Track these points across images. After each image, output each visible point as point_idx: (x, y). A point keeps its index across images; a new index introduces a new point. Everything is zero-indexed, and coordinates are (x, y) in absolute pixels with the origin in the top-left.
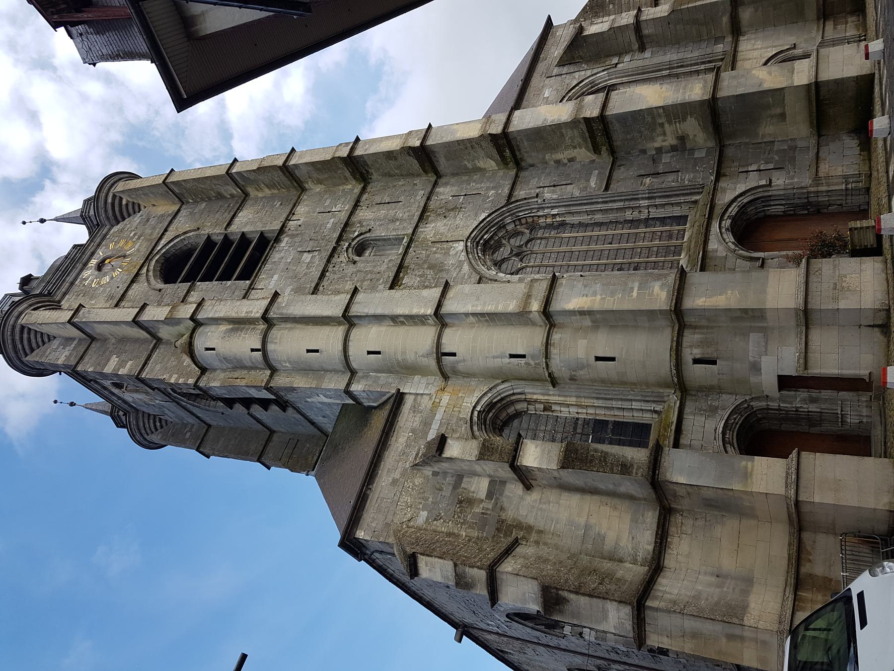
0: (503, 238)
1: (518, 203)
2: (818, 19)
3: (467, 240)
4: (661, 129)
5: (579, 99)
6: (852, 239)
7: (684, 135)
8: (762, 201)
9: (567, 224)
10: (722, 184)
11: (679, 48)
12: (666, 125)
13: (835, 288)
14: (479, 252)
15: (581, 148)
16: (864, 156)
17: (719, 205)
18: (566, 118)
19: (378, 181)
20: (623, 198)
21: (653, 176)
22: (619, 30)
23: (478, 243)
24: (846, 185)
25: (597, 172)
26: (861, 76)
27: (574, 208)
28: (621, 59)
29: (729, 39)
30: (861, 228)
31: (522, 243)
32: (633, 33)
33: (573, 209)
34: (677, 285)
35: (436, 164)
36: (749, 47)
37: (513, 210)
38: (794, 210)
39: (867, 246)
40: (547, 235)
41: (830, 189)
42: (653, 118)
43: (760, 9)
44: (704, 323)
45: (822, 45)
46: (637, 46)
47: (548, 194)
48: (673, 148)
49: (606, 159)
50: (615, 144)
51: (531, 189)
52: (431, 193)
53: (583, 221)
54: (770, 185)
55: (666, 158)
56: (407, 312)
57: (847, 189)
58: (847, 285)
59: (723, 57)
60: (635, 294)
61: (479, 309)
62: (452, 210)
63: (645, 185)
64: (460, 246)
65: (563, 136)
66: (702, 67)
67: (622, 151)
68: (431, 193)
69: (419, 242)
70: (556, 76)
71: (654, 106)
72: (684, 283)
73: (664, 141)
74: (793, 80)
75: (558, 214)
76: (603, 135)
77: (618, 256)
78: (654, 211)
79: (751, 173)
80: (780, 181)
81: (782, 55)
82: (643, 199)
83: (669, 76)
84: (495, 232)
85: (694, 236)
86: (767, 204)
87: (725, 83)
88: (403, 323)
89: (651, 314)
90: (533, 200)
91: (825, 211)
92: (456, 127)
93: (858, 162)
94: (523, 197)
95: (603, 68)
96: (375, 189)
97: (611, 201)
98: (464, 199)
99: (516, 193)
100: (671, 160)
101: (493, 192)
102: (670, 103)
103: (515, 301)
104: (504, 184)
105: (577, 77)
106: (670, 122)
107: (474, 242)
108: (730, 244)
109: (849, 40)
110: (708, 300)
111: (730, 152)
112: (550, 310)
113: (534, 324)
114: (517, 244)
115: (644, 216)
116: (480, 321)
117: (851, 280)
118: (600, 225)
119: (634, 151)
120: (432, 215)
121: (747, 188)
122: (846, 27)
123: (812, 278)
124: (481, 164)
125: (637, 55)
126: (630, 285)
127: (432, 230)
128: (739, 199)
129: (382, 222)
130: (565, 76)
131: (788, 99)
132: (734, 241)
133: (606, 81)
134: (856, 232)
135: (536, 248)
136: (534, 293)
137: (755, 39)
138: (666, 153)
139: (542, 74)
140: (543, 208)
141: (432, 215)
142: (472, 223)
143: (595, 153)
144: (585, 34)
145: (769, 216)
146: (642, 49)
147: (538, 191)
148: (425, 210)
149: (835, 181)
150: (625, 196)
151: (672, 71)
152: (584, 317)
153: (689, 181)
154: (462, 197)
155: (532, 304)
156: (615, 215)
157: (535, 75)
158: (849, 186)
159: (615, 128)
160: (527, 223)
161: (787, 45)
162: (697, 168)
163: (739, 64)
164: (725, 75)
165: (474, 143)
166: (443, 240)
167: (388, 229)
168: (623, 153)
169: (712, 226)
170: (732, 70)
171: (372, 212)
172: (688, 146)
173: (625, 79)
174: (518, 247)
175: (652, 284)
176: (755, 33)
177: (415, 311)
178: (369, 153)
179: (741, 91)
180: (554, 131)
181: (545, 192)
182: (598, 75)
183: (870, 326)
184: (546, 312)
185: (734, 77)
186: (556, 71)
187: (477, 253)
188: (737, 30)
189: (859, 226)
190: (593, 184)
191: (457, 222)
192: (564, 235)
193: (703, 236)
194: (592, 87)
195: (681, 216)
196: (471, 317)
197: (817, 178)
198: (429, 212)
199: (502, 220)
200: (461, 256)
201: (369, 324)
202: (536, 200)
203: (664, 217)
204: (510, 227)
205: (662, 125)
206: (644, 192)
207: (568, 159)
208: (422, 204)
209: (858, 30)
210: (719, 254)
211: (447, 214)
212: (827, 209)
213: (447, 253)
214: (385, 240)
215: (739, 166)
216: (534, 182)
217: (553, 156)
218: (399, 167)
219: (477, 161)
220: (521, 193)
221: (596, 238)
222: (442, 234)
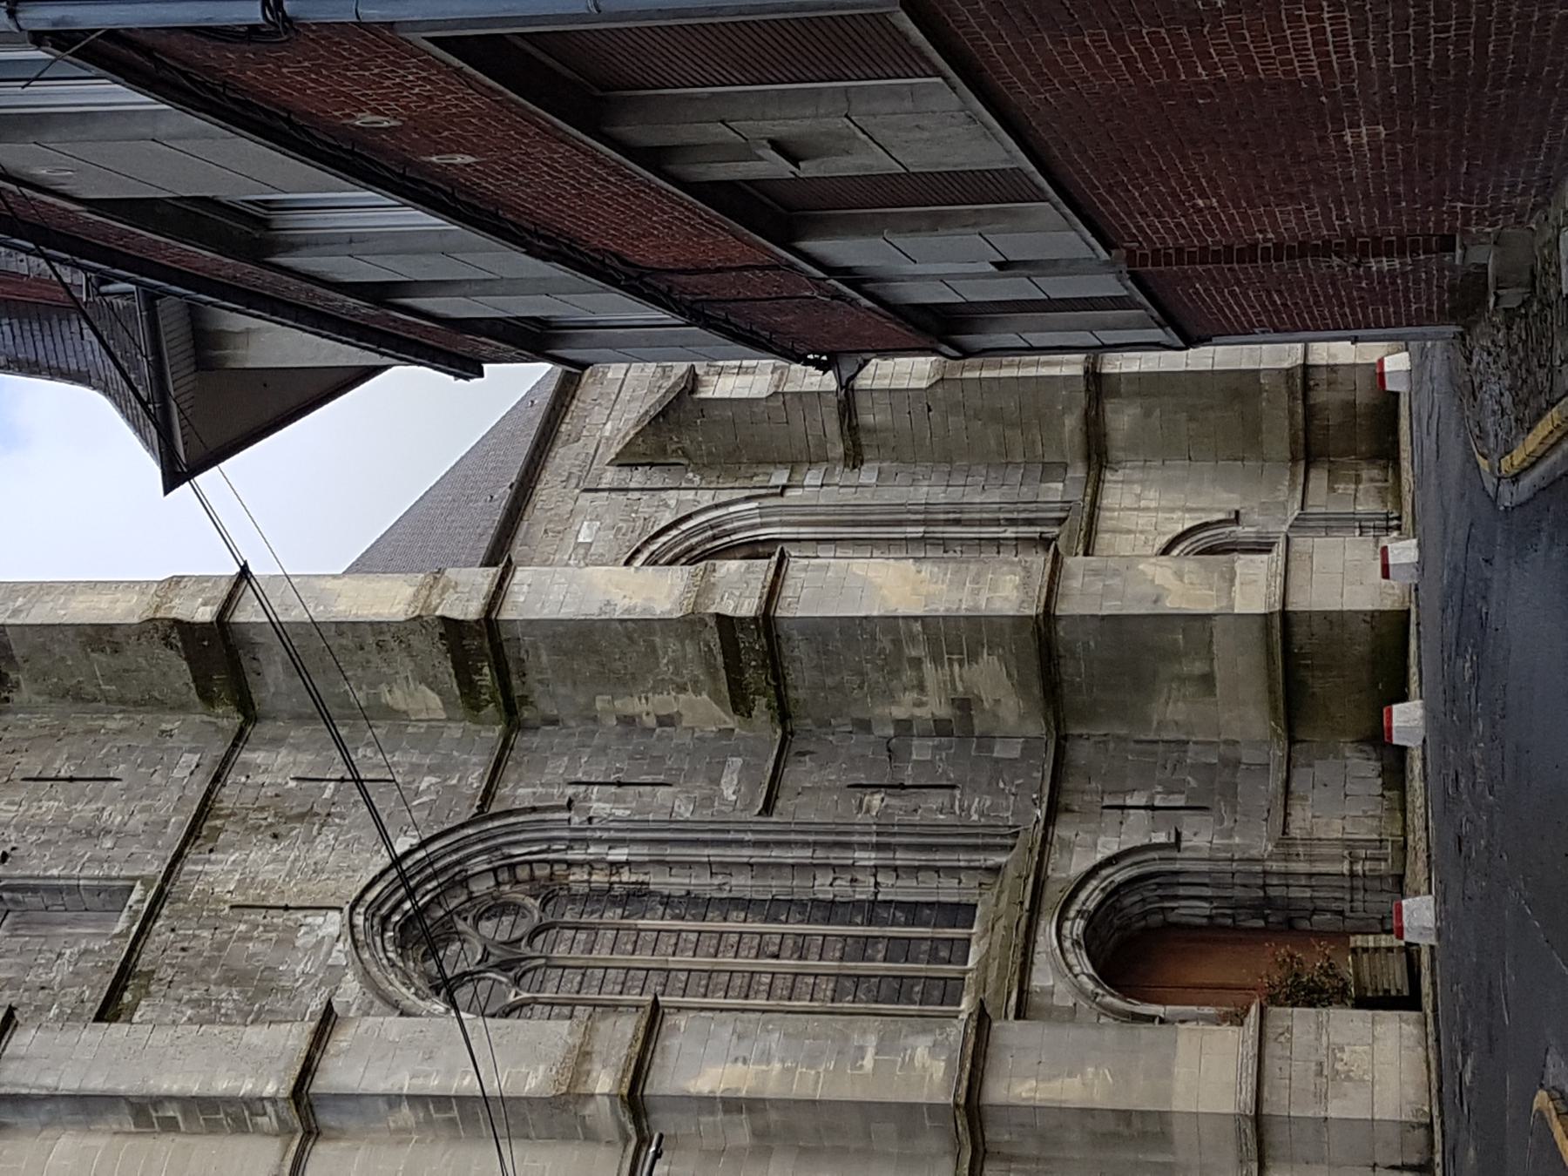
0: (459, 914)
1: (512, 820)
2: (1294, 460)
3: (353, 908)
4: (914, 674)
5: (702, 565)
6: (1357, 974)
7: (970, 696)
8: (1159, 885)
9: (651, 894)
10: (1062, 831)
11: (950, 474)
12: (928, 666)
13: (1320, 1073)
14: (390, 947)
15: (697, 692)
16: (1390, 799)
17: (1059, 880)
18: (668, 607)
19: (31, 709)
20: (811, 838)
21: (889, 791)
22: (796, 399)
23: (385, 919)
24: (1351, 863)
25: (738, 761)
26: (1382, 613)
27: (676, 851)
28: (797, 477)
29: (1078, 471)
30: (1376, 949)
31: (517, 934)
32: (835, 416)
33: (671, 852)
34: (970, 1045)
35: (251, 678)
36: (1128, 502)
37: (494, 837)
38: (1233, 917)
39: (1389, 991)
40: (594, 919)
41: (1315, 870)
42: (896, 642)
43: (1157, 412)
44: (1031, 1148)
45: (1301, 524)
46: (840, 450)
47: (601, 805)
48: (941, 728)
49: (763, 728)
50: (792, 694)
51: (551, 785)
52: (226, 763)
53: (695, 891)
54: (1177, 845)
55: (921, 750)
56: (195, 1089)
57: (1353, 875)
58: (1346, 1068)
59: (1063, 515)
60: (868, 1063)
61: (433, 1084)
62: (301, 817)
63: (868, 811)
64: (332, 924)
65: (654, 650)
66: (1010, 532)
67: (809, 716)
68: (226, 763)
69: (186, 902)
70: (611, 490)
71: (900, 612)
72: (987, 1046)
73: (920, 704)
74: (1231, 600)
75: (628, 863)
76: (764, 666)
77: (797, 991)
78: (890, 882)
79: (1132, 811)
80: (1200, 837)
81: (1206, 534)
82: (864, 846)
83: (923, 540)
84: (437, 896)
85: (996, 951)
86: (1170, 892)
87: (1076, 584)
88: (170, 1125)
89: (907, 1116)
90: (557, 816)
91: (1305, 924)
92: (330, 584)
93: (1378, 812)
94: (526, 804)
95: (747, 493)
96: (17, 734)
97: (779, 844)
98: (337, 790)
99: (504, 791)
100: (934, 756)
101: (434, 780)
102: (941, 612)
103: (542, 1068)
104: (465, 762)
105: (672, 503)
106: (937, 660)
107: (373, 915)
108: (1084, 979)
109: (1363, 524)
110: (1041, 1085)
111: (1081, 753)
112: (646, 1092)
113: (590, 1136)
114: (503, 936)
115: (863, 894)
116: (429, 1121)
117: (1354, 1057)
118: (745, 905)
119: (840, 720)
120: (231, 828)
121: (1124, 847)
122: (1356, 490)
123: (1272, 1048)
124: (396, 697)
125: (840, 475)
126: (856, 1040)
127: (229, 872)
128: (1104, 873)
129: (53, 835)
130: (637, 495)
131: (1221, 643)
132: (1091, 971)
133: (753, 527)
134: (1365, 956)
135: (560, 951)
136: (598, 1046)
137: (1142, 482)
138: (921, 736)
139: (568, 478)
140: (586, 842)
141: (231, 828)
142: (367, 862)
143: (735, 710)
144: (703, 395)
145: (1177, 926)
146: (854, 459)
147: (570, 791)
148: (206, 808)
149: (1324, 851)
150: (817, 833)
151: (931, 529)
152: (736, 1118)
153: (981, 814)
154: (332, 785)
155: (594, 1074)
156: (789, 883)
157: (546, 476)
158: (1358, 868)
159: (796, 653)
160: (532, 878)
161: (1219, 510)
162: (1001, 785)
163: (1103, 539)
164: (1075, 563)
165: (388, 637)
166: (271, 902)
167: (72, 860)
168: (809, 721)
169: (1040, 931)
170: (1086, 554)
171: (12, 803)
172: (979, 725)
173: (806, 532)
174: (504, 943)
175: (911, 1040)
176: (1143, 467)
177: (222, 1086)
178: (29, 621)
179: (1110, 607)
180: (630, 638)
181: (594, 797)
182: (732, 509)
183: (1393, 1167)
184: (635, 1102)
185: (1096, 572)
186: (610, 476)
187: (385, 950)
188: (1098, 455)
189: (1371, 944)
190: (729, 793)
191: (318, 856)
192: (641, 923)
193: (1019, 954)
194: (715, 538)
195: (958, 904)
196: (405, 1109)
197: (1285, 837)
198: (218, 817)
199: (458, 862)
200: (334, 954)
201: (44, 1126)
202: (566, 815)
203: (917, 903)
204: (481, 887)
205: (917, 663)
206: (866, 829)
207: (658, 717)
208: (196, 792)
209: (1384, 503)
210: (1056, 1001)
211: (282, 829)
212: (1309, 920)
213: (286, 941)
214: (59, 890)
215: (1103, 792)
216: (558, 767)
217: (618, 703)
218: (114, 677)
219: (384, 688)
220: (521, 791)
221: (734, 939)
222: (268, 887)
